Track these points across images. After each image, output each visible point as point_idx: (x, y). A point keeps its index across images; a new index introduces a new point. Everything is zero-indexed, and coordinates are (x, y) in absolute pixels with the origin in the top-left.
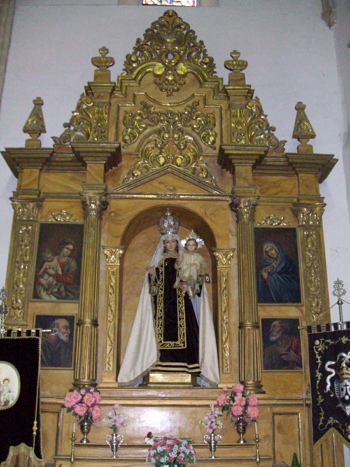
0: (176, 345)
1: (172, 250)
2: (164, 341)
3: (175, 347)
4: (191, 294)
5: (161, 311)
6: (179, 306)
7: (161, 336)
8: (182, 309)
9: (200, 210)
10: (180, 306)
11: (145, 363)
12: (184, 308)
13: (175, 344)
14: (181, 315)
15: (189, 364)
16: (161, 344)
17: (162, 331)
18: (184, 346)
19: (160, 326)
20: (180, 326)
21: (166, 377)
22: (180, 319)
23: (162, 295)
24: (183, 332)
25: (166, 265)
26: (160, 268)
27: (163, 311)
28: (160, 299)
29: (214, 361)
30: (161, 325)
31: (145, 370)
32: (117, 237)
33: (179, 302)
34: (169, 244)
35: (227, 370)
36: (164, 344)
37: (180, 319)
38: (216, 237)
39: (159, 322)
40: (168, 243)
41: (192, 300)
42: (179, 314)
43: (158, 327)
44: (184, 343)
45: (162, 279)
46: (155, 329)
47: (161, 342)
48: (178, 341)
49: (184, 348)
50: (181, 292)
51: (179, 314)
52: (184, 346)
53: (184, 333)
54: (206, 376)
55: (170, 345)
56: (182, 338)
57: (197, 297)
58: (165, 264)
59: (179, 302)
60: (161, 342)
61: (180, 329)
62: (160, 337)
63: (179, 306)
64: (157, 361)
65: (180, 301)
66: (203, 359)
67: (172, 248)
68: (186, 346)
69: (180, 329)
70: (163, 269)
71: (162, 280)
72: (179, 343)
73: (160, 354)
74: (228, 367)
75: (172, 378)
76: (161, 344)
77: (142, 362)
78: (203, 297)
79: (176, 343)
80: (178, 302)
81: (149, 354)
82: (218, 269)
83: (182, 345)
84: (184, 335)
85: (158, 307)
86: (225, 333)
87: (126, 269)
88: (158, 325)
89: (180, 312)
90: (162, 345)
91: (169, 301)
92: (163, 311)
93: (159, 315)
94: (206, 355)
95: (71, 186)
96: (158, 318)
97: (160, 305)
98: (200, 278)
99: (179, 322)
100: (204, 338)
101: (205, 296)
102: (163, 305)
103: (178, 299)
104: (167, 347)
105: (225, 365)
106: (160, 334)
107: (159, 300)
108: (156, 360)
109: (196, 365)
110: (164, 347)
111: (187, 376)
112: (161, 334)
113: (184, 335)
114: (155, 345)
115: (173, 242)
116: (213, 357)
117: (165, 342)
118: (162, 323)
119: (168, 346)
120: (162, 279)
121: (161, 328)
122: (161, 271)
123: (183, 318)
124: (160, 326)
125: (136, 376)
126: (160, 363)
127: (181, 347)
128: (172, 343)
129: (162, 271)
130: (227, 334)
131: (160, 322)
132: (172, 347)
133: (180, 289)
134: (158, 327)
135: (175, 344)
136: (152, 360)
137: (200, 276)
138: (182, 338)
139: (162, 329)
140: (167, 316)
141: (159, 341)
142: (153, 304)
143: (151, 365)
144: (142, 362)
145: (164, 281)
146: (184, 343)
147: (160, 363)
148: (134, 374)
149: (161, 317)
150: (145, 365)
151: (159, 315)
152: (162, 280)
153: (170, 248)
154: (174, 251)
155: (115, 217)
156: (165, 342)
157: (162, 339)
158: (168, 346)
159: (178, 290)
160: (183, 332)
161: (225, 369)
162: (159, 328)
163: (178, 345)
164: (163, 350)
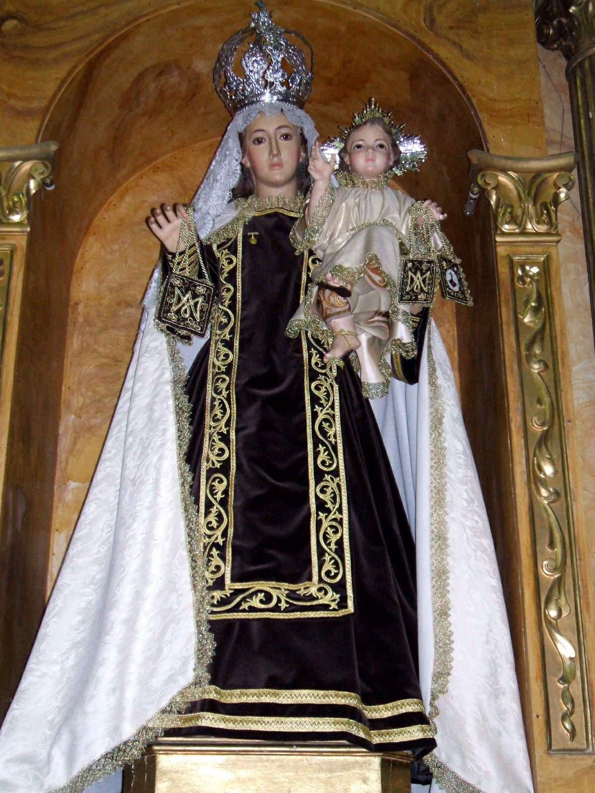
0: (299, 599)
1: (278, 175)
2: (234, 579)
3: (291, 609)
4: (370, 374)
5: (225, 438)
6: (315, 415)
7: (223, 557)
8: (331, 433)
9: (405, 11)
10: (321, 416)
11: (131, 693)
12: (338, 427)
13: (292, 595)
14: (323, 456)
15: (368, 700)
16: (218, 594)
17: (225, 534)
18: (343, 604)
19: (216, 508)
20: (321, 506)
21: (244, 773)
22: (319, 475)
23: (230, 366)
24: (334, 538)
25: (253, 241)
26: (222, 256)
27: (233, 436)
28: (223, 386)
29: (496, 694)
30: (223, 503)
31: (128, 731)
32: (24, 114)
33: (315, 400)
34: (264, 146)
35: (573, 733)
36: (237, 592)
37: (319, 475)
38: (484, 117)
39: (212, 490)
40: (259, 141)
41: (376, 405)
42: (316, 454)
43: (207, 513)
44: (340, 587)
45: (233, 298)
46: (188, 520)
47: (219, 584)
48: (310, 579)
49: (341, 613)
50: (322, 356)
51: (316, 454)
52: (343, 604)
53: (340, 543)
54: (456, 766)
55: (268, 597)
56: (328, 566)
57: (399, 385)
58: (246, 238)
59: (315, 400)
60: (219, 584)
61: (319, 523)
62: (216, 561)
63: (315, 415)
64: (197, 683)
65: (321, 394)
66: (442, 674)
67: (280, 165)
68: (350, 603)
69: (319, 523)
70: (238, 260)
71: (232, 307)
72: (313, 590)
73: (210, 646)
74: (578, 718)
75: (280, 776)
76: (218, 594)
77: (119, 687)
78: (433, 383)
79: (301, 588)
80: (307, 398)
81: (155, 655)
82: (501, 251)
83: (330, 598)
84: (340, 551)
85: (208, 421)
86: (552, 545)
87: (81, 308)
88: (209, 505)
89: (317, 442)
90: (223, 602)
91: (264, 393)
92: (233, 436)
93: (213, 458)
94: (458, 655)
95: (16, 304)
96: (210, 472)
97: (218, 411)
98: (418, 279)
99: (313, 490)
100: (441, 574)
101: (439, 373)
102: (232, 410)
103: (308, 387)
104: (252, 609)
105: (560, 706)
106: (216, 545)
107: (217, 390)
108: (190, 676)
109: (407, 706)
110: (236, 609)
111: (361, 765)
112: (221, 549)
113: (340, 551)
114: (188, 597)
115: (286, 137)
116: (493, 675)
117: (239, 586)
118: (226, 492)
119: (255, 602)
120: (233, 298)
121: (220, 517)
122: (228, 268)
123: (336, 473)
124: (216, 508)
125: (83, 762)
126: (212, 693)
127: (325, 607)
128: (279, 590)
129: (234, 270)
130: (558, 549)
131: (220, 488)
132: (276, 609)
133: (318, 341)
134: (207, 513)
135: (292, 595)
136: (171, 679)
137: (417, 266)
138: (328, 566)
139: (229, 519)
140: (252, 460)
141: (210, 578)
142: (185, 399)
143: (164, 703)
144: (119, 687)
145: (239, 305)
146: (340, 587)
147: (212, 693)
148: (71, 757)
149: (225, 468)
150: (129, 707)
151: (210, 456)
152: (232, 307)
153: (272, 166)
154: (288, 181)
155: (21, 34)
156: (239, 586)
157: (227, 570)
158: (255, 602)
159: (310, 346)
160: (334, 538)
161: (562, 729)
162: (212, 518)
163: (312, 598)
164: (230, 623)
